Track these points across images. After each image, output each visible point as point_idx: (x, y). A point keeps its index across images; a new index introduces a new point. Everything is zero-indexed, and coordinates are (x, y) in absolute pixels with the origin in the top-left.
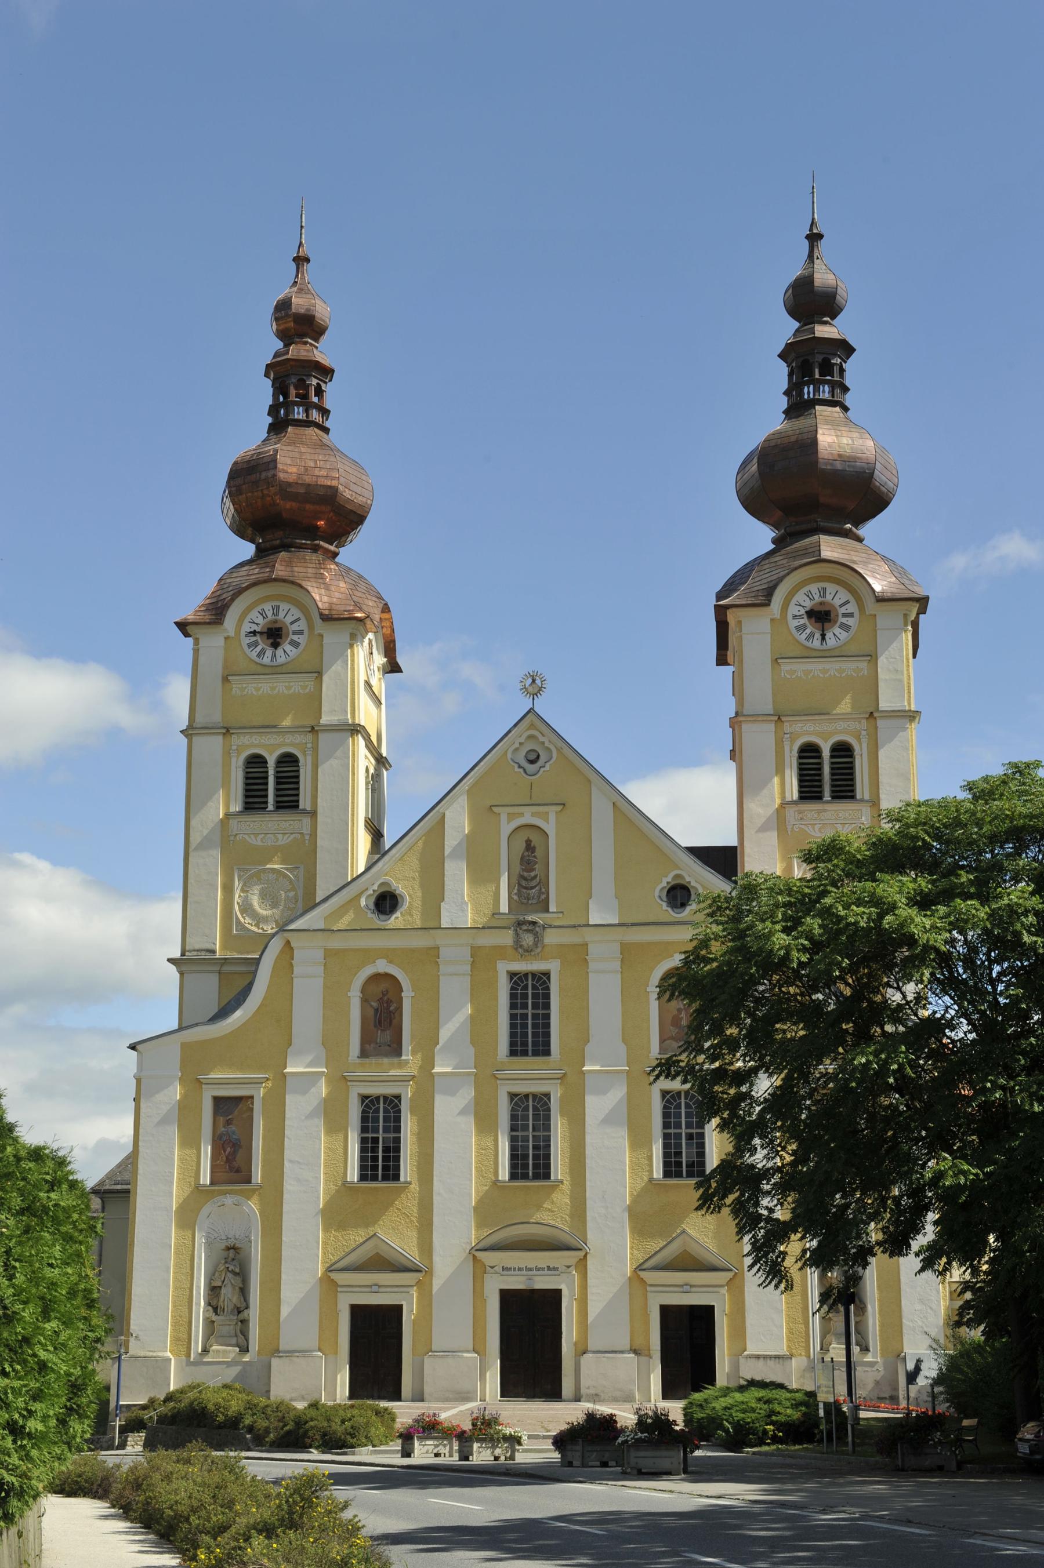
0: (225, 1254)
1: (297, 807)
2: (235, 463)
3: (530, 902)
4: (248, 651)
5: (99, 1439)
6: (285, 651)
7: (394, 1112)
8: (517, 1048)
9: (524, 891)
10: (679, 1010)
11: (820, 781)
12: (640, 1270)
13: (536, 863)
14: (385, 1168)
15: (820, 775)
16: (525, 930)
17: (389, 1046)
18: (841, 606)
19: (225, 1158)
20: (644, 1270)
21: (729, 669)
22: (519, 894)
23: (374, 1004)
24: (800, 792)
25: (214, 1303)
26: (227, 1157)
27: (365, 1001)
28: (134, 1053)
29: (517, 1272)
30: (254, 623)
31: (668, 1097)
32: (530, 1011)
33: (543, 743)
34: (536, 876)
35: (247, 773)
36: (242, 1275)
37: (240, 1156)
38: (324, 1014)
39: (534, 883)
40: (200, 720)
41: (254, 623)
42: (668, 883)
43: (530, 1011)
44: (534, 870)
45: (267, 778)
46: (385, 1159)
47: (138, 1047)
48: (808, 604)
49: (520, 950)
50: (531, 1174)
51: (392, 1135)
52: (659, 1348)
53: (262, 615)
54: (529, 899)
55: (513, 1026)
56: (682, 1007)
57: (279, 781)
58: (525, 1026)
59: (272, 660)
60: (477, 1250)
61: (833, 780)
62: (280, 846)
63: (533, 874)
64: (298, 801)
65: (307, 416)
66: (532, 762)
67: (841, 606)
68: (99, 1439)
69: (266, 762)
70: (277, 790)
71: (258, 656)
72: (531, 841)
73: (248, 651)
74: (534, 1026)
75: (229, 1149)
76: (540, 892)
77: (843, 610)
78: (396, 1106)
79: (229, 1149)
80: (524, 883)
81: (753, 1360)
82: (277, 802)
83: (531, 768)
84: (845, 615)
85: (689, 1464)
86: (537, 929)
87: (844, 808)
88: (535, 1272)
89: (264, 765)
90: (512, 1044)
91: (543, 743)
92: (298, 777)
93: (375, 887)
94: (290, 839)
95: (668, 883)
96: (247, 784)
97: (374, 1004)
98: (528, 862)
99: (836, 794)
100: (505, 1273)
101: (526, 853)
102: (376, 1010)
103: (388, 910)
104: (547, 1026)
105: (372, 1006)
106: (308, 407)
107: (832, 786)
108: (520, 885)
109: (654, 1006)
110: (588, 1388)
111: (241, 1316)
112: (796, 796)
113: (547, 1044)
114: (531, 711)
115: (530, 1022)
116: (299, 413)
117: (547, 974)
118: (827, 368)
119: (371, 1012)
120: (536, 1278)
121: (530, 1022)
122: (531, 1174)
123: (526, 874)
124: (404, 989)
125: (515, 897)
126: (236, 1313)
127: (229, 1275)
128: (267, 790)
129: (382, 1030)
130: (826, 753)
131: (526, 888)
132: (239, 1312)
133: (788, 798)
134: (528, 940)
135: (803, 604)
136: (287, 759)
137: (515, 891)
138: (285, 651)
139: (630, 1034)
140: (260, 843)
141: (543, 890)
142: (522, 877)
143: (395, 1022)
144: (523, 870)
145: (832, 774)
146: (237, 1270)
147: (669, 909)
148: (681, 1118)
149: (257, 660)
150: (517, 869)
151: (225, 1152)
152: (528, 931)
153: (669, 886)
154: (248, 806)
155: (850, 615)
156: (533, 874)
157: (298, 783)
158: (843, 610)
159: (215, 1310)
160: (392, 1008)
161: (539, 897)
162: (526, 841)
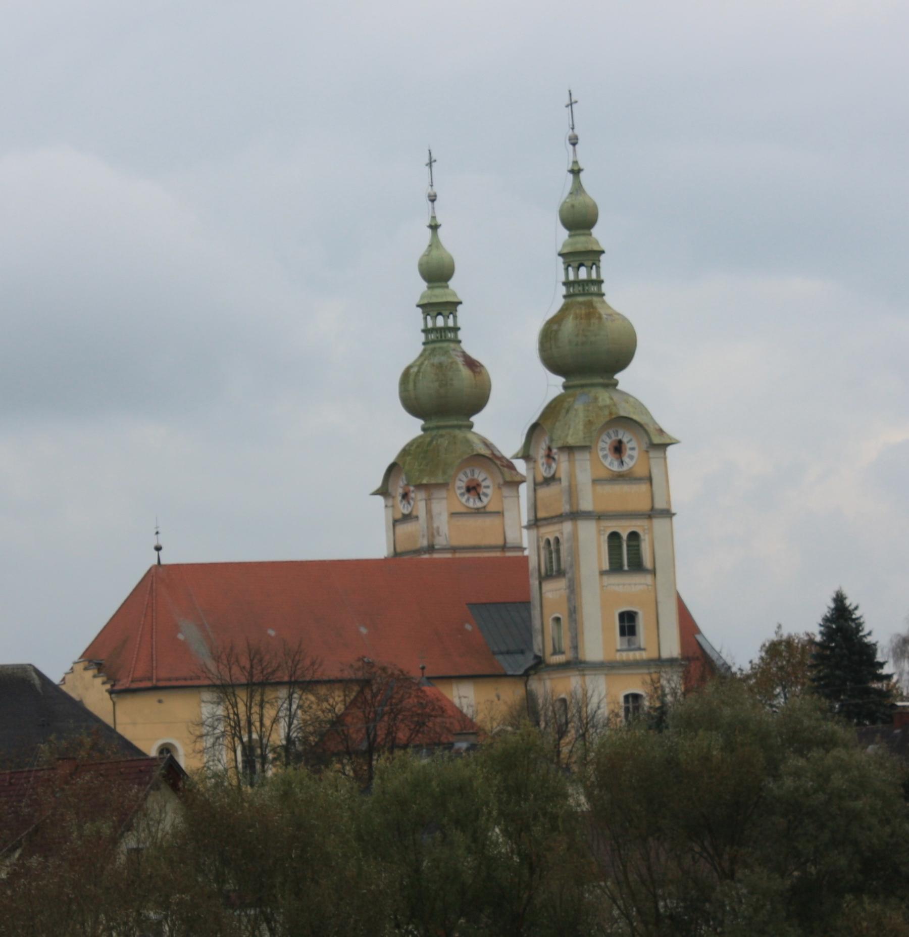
4: (460, 498)
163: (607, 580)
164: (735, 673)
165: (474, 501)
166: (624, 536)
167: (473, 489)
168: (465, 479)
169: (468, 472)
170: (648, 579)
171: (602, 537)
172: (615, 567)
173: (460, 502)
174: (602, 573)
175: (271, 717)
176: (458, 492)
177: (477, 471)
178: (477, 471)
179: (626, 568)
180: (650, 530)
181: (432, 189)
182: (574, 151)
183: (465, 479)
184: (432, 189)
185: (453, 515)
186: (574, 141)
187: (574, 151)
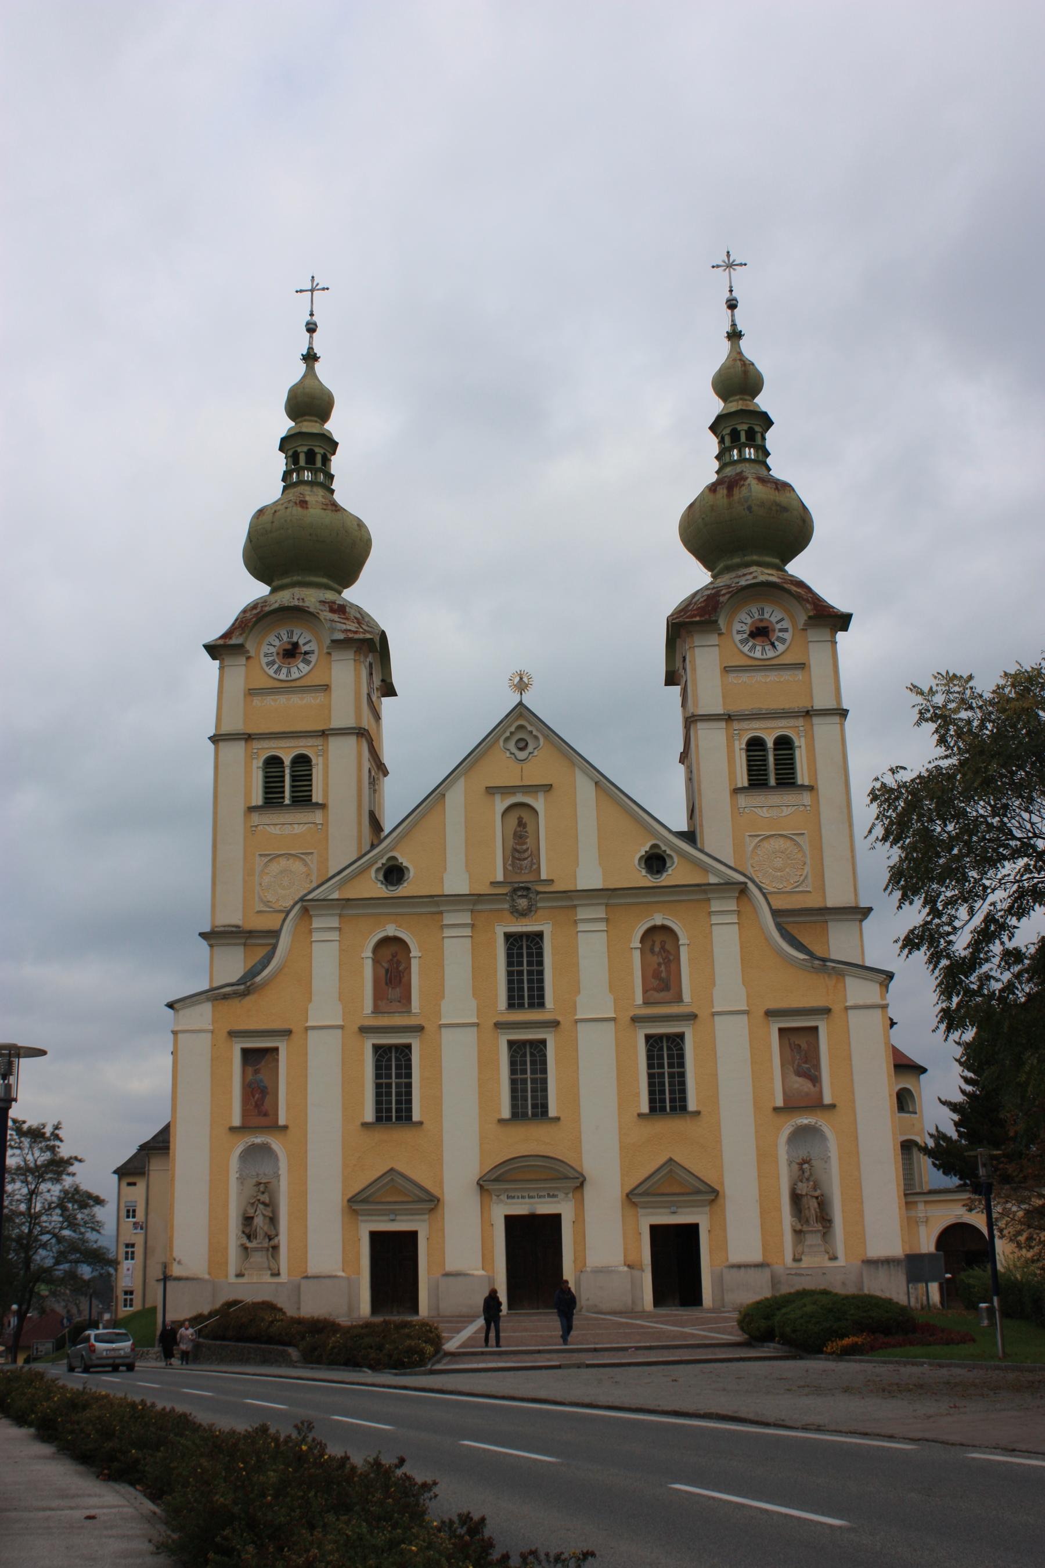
0: (256, 1189)
1: (311, 800)
2: (261, 512)
3: (523, 872)
4: (266, 669)
5: (148, 1351)
6: (298, 668)
7: (405, 1061)
8: (514, 1001)
9: (518, 862)
10: (659, 964)
11: (765, 770)
12: (632, 1195)
13: (527, 837)
14: (530, 997)
15: (765, 765)
16: (520, 896)
17: (399, 1002)
18: (777, 622)
19: (254, 1104)
20: (636, 1194)
21: (677, 689)
22: (513, 865)
23: (386, 965)
24: (749, 780)
25: (247, 1231)
26: (256, 1103)
27: (376, 961)
28: (171, 1011)
29: (520, 1200)
30: (271, 645)
31: (651, 1041)
32: (525, 967)
33: (531, 732)
34: (528, 849)
35: (266, 772)
36: (271, 1205)
37: (268, 1101)
38: (340, 975)
39: (526, 855)
40: (225, 729)
41: (271, 645)
42: (646, 852)
43: (525, 967)
44: (526, 843)
45: (283, 776)
46: (398, 1102)
47: (176, 1006)
48: (747, 629)
49: (515, 914)
50: (530, 1113)
51: (404, 1080)
52: (650, 1263)
53: (278, 638)
54: (522, 869)
55: (510, 982)
56: (661, 961)
57: (294, 778)
58: (521, 981)
59: (287, 676)
60: (484, 1181)
61: (776, 769)
62: (295, 834)
63: (525, 847)
64: (311, 796)
65: (316, 479)
66: (521, 749)
67: (777, 622)
68: (148, 1351)
69: (282, 763)
70: (292, 786)
71: (275, 672)
72: (522, 818)
73: (266, 669)
74: (530, 981)
75: (257, 1096)
76: (532, 864)
77: (779, 626)
78: (407, 1055)
79: (257, 1096)
80: (517, 855)
81: (735, 1270)
82: (293, 797)
83: (522, 755)
84: (781, 630)
85: (861, 964)
86: (531, 895)
87: (788, 798)
88: (536, 1200)
89: (280, 766)
90: (510, 998)
91: (531, 732)
92: (311, 775)
93: (384, 861)
94: (304, 829)
95: (646, 852)
96: (266, 782)
97: (386, 965)
98: (521, 837)
99: (779, 781)
100: (509, 1201)
101: (519, 829)
102: (387, 971)
103: (395, 882)
104: (541, 981)
105: (383, 967)
106: (315, 471)
107: (777, 774)
108: (513, 857)
109: (637, 955)
110: (588, 1299)
111: (272, 1243)
112: (746, 784)
113: (542, 997)
114: (520, 704)
115: (525, 977)
116: (307, 475)
117: (540, 935)
118: (751, 435)
119: (383, 972)
120: (538, 1206)
121: (525, 977)
122: (530, 1113)
123: (518, 847)
124: (412, 950)
125: (510, 868)
126: (267, 1240)
127: (261, 1206)
128: (283, 787)
129: (393, 988)
130: (770, 744)
131: (519, 859)
132: (270, 1240)
133: (740, 785)
134: (523, 903)
135: (745, 621)
136: (301, 760)
137: (510, 862)
138: (298, 668)
139: (616, 984)
140: (278, 832)
141: (535, 861)
142: (515, 850)
143: (404, 980)
144: (516, 844)
145: (776, 764)
146: (267, 1201)
147: (648, 875)
148: (663, 1059)
149: (274, 676)
150: (511, 842)
151: (254, 1097)
152: (522, 896)
153: (648, 854)
154: (268, 801)
155: (785, 630)
156: (525, 847)
157: (311, 780)
158: (779, 626)
159: (249, 1237)
160: (401, 968)
161: (531, 867)
162: (518, 819)
163: (742, 800)
164: (1039, 946)
165: (764, 649)
166: (287, 762)
167: (761, 633)
168: (749, 621)
169: (754, 610)
170: (806, 798)
171: (255, 762)
172: (757, 781)
173: (742, 652)
174: (736, 791)
175: (796, 1124)
176: (738, 637)
177: (768, 610)
178: (768, 610)
179: (772, 782)
180: (324, 753)
181: (731, 294)
182: (311, 337)
183: (277, 643)
184: (731, 294)
185: (727, 670)
186: (311, 328)
187: (311, 337)
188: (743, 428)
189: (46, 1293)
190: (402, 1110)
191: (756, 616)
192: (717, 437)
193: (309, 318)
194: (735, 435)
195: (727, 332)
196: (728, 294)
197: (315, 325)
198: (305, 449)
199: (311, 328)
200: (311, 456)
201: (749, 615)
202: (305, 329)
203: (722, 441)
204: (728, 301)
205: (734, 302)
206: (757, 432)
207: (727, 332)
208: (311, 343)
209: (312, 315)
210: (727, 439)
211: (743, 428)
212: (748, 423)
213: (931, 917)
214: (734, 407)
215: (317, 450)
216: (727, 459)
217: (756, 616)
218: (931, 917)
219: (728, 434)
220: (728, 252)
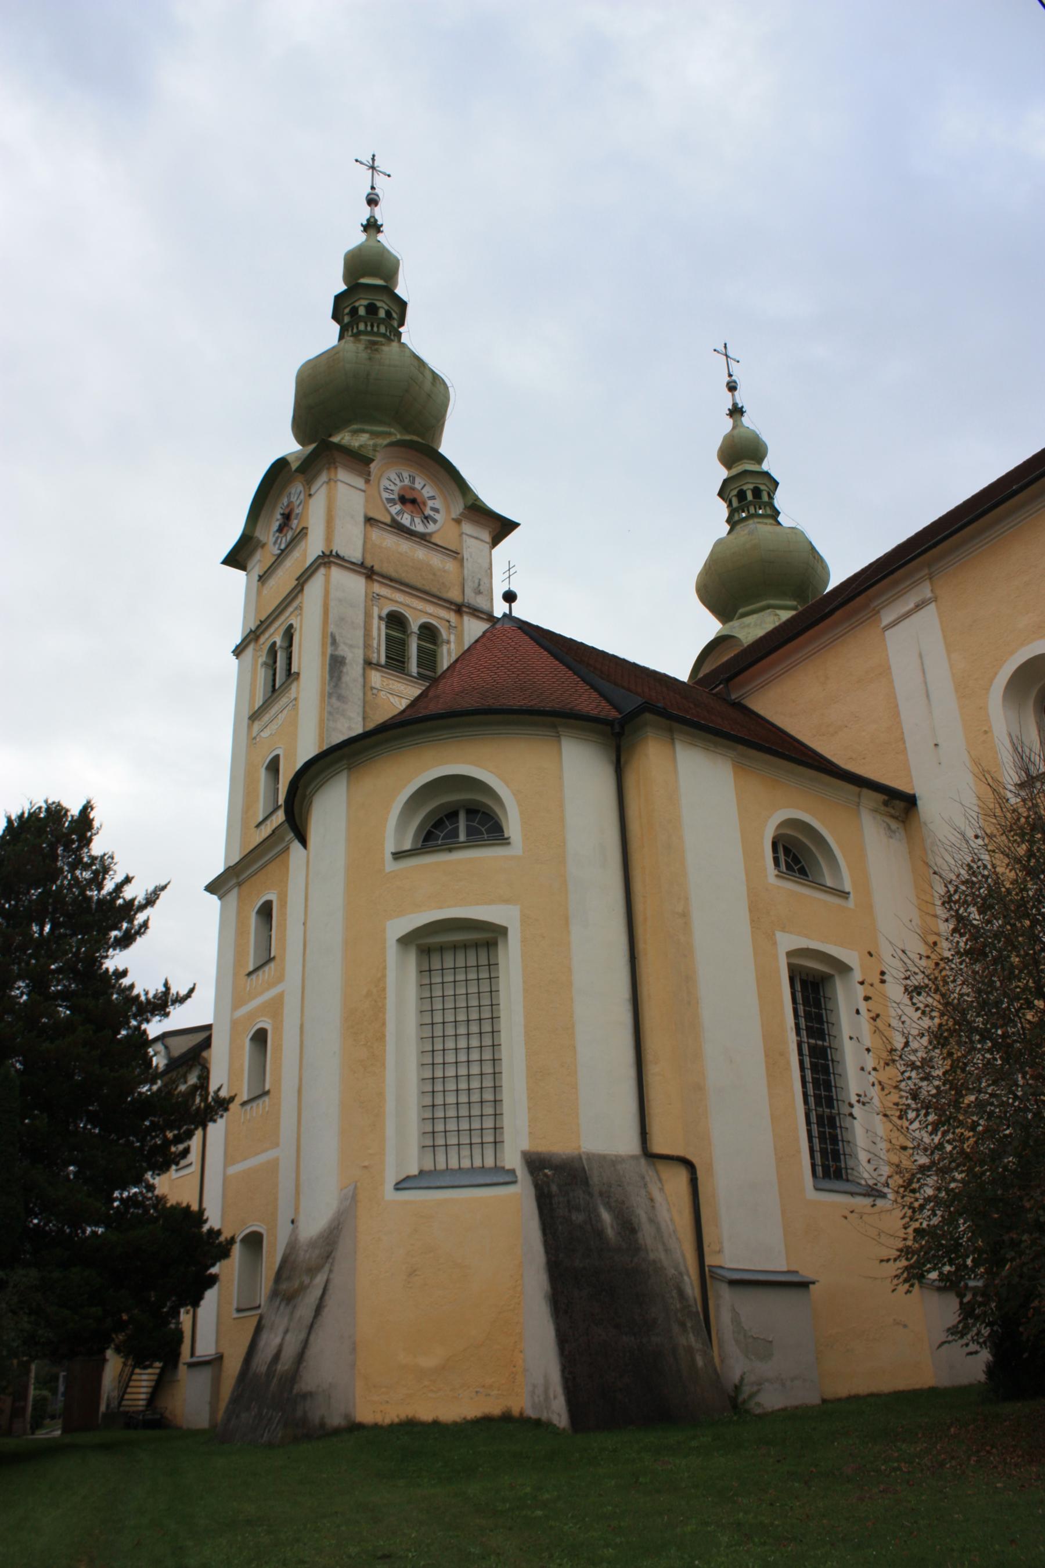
65: (766, 512)
182: (733, 395)
187: (733, 395)
188: (748, 488)
189: (938, 1447)
190: (816, 1078)
191: (407, 482)
192: (726, 502)
193: (729, 379)
194: (741, 495)
195: (729, 410)
196: (727, 379)
197: (735, 382)
198: (751, 486)
199: (732, 387)
200: (757, 493)
201: (399, 477)
202: (726, 390)
203: (730, 505)
204: (728, 383)
205: (733, 384)
206: (763, 490)
207: (729, 410)
208: (733, 399)
209: (730, 375)
210: (735, 503)
211: (748, 488)
212: (735, 488)
213: (355, 327)
214: (735, 471)
215: (762, 487)
216: (736, 518)
217: (407, 482)
218: (355, 327)
219: (735, 496)
220: (725, 344)
